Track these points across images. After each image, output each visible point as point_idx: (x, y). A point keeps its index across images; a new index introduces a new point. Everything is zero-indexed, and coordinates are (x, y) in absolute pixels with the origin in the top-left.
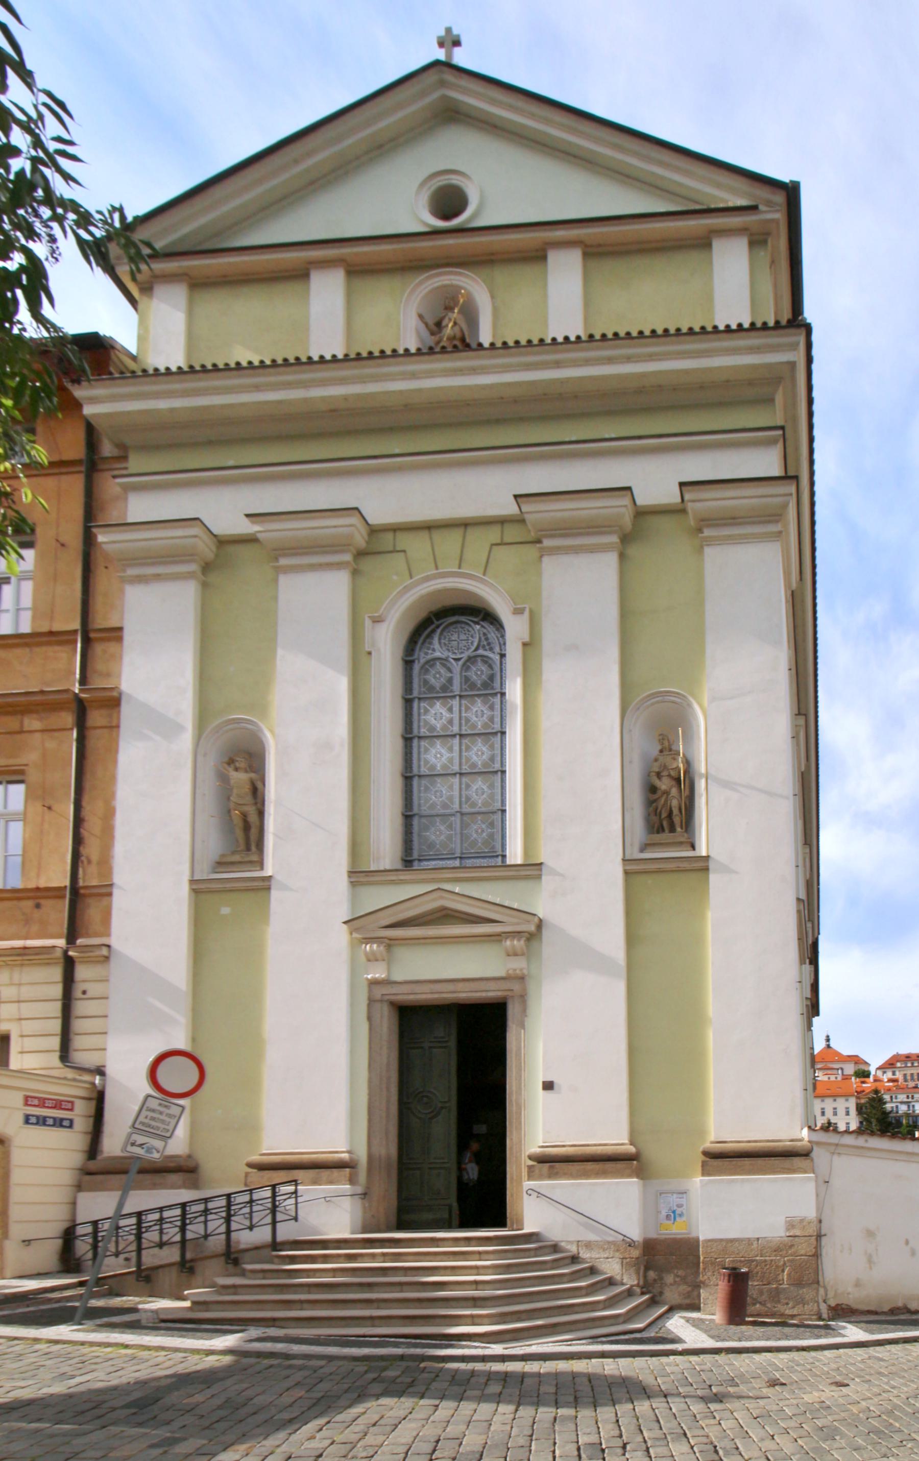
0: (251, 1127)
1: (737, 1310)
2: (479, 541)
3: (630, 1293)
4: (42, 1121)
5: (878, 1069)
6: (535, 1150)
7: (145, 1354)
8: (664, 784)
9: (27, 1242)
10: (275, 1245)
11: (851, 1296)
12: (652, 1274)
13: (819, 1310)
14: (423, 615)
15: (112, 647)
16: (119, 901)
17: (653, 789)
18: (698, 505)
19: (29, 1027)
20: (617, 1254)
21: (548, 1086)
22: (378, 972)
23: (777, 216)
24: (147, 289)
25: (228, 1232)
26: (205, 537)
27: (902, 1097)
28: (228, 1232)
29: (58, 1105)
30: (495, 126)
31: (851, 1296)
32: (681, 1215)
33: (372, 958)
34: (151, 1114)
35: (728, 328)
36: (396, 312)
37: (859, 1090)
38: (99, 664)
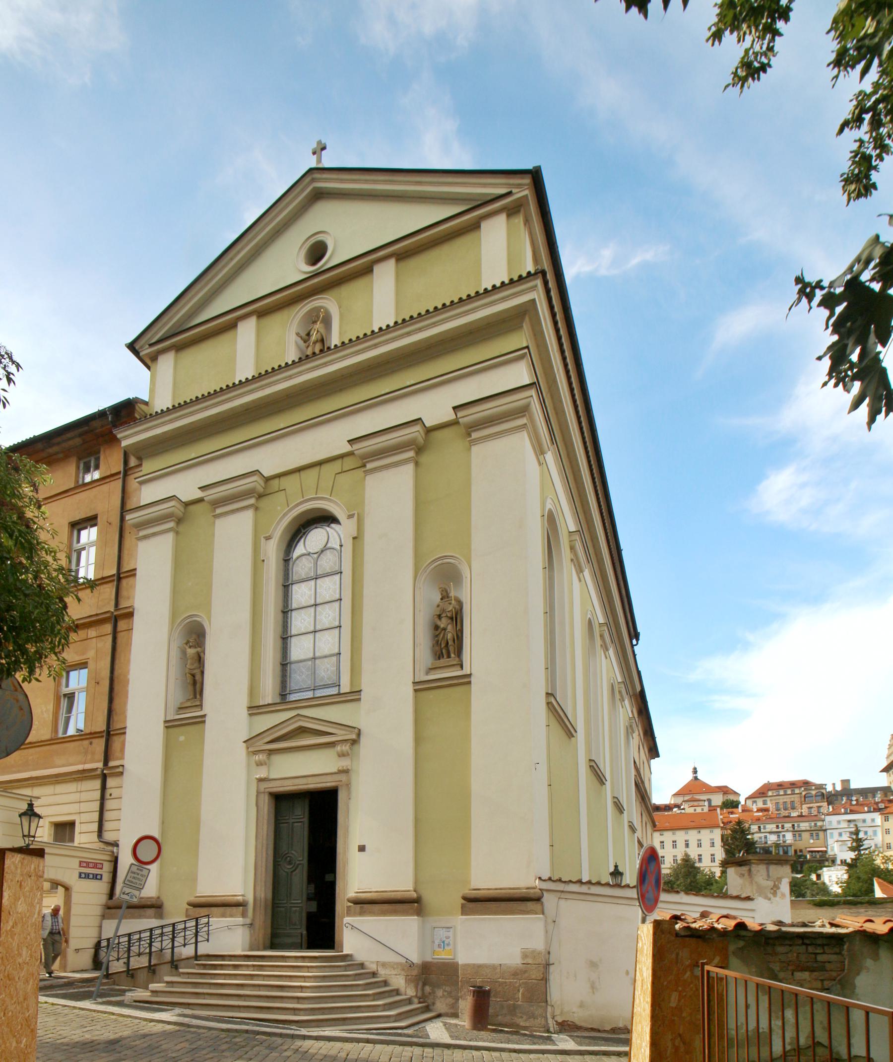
0: (193, 879)
1: (481, 1017)
2: (329, 471)
3: (409, 1001)
4: (87, 876)
5: (747, 799)
6: (351, 894)
7: (121, 1019)
8: (442, 624)
9: (77, 950)
10: (196, 957)
11: (575, 1015)
12: (428, 989)
13: (547, 1023)
14: (296, 527)
15: (131, 579)
16: (129, 737)
17: (436, 627)
18: (466, 419)
19: (85, 817)
20: (403, 973)
21: (362, 849)
22: (262, 773)
23: (526, 192)
24: (154, 358)
25: (173, 948)
26: (178, 506)
27: (771, 827)
28: (173, 948)
29: (95, 866)
30: (345, 194)
31: (575, 1015)
32: (448, 945)
33: (259, 764)
34: (133, 875)
35: (461, 300)
36: (284, 338)
37: (725, 820)
38: (124, 593)
